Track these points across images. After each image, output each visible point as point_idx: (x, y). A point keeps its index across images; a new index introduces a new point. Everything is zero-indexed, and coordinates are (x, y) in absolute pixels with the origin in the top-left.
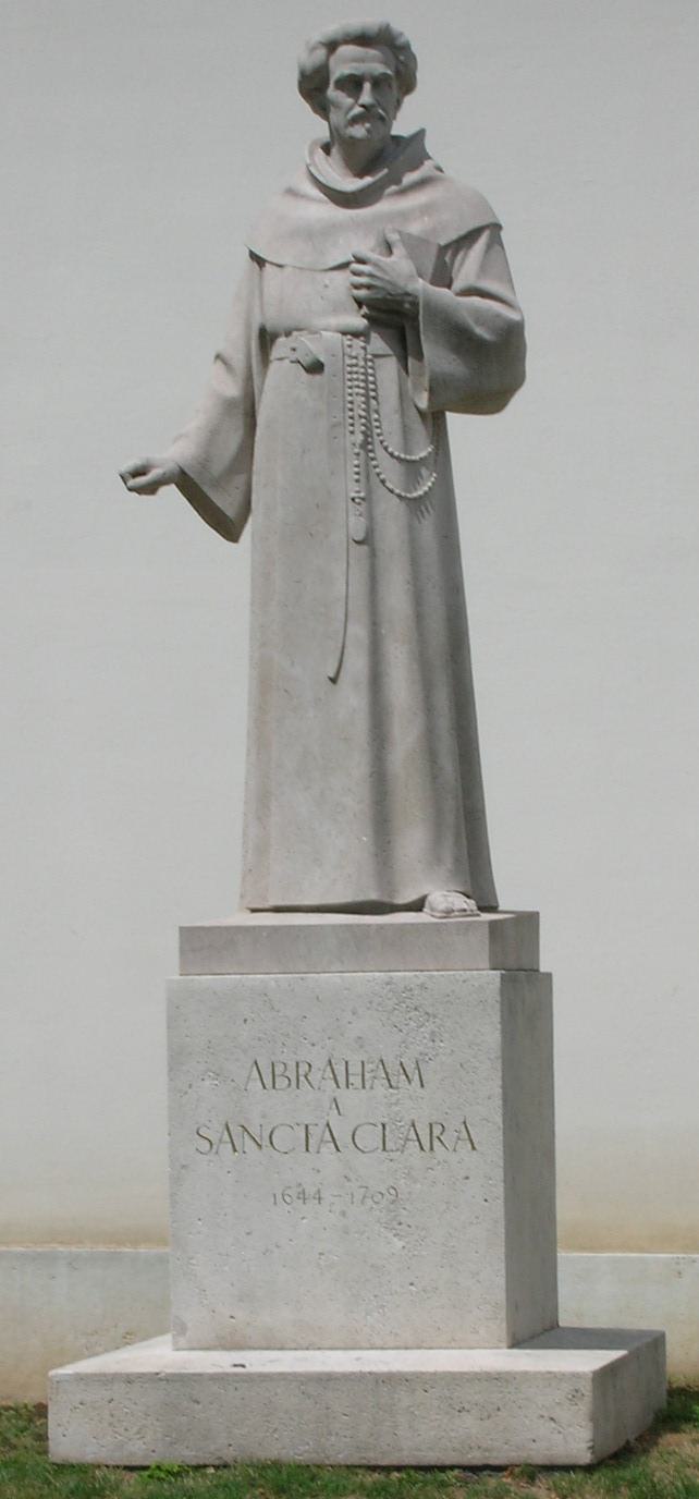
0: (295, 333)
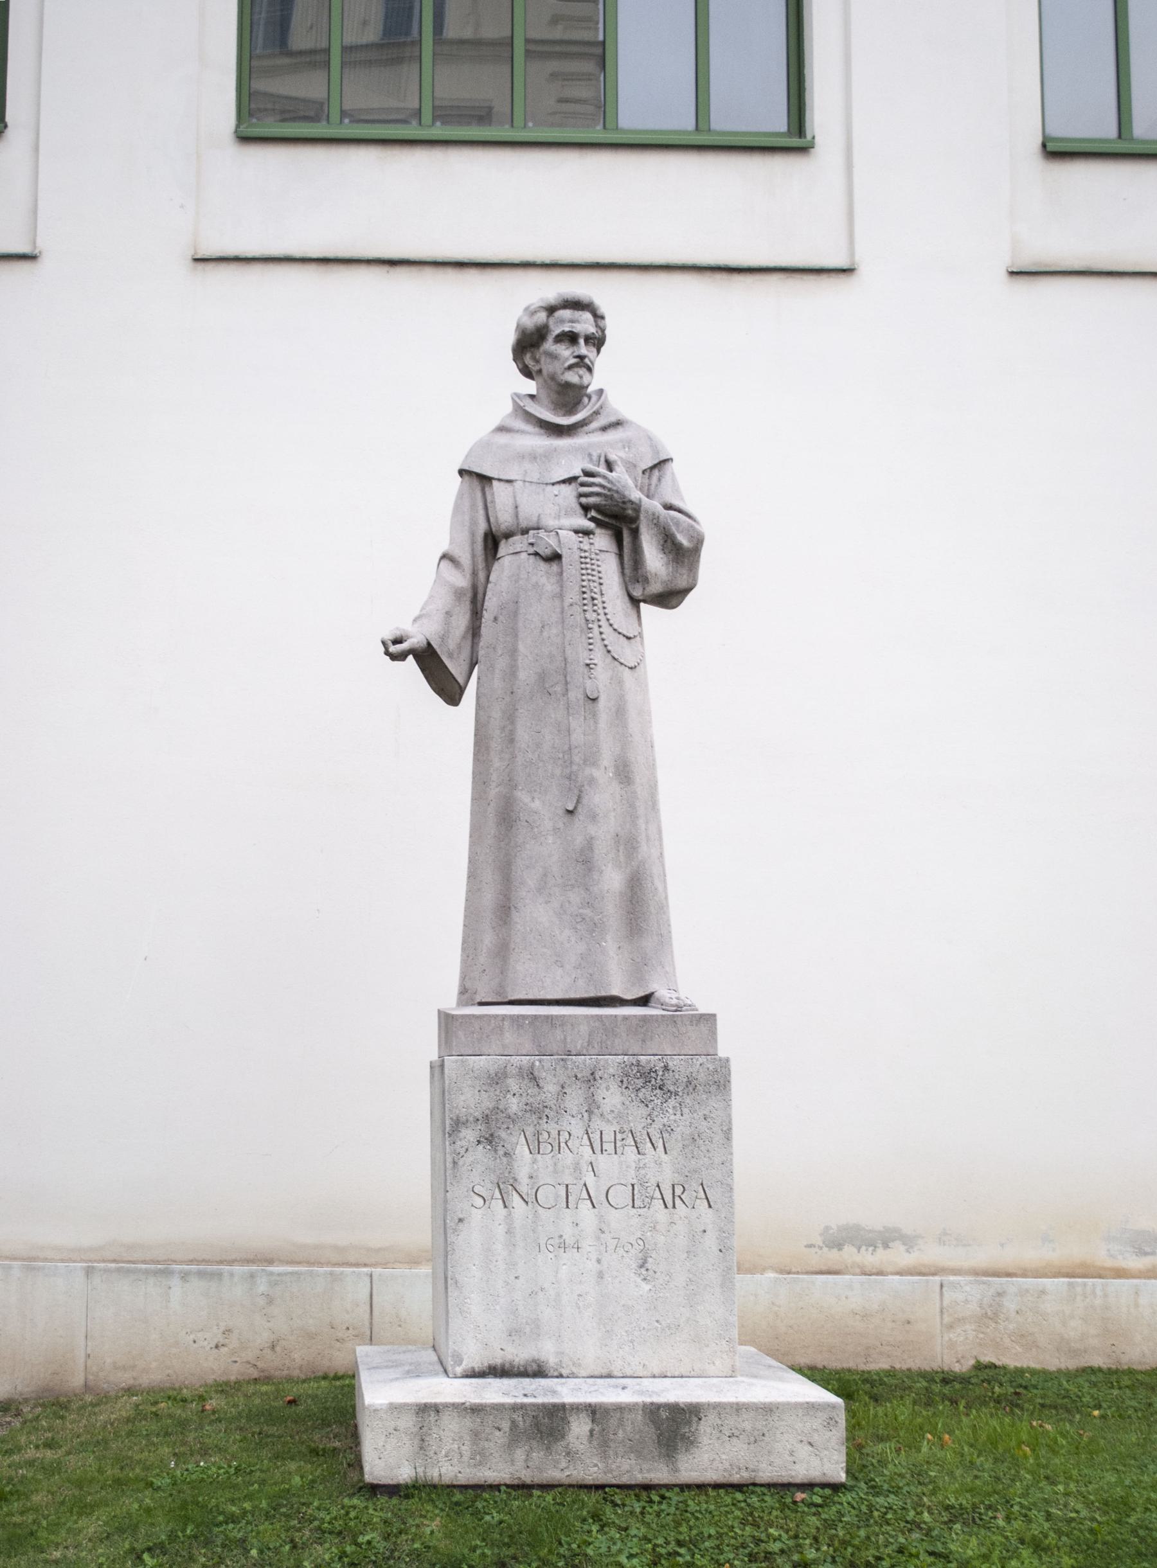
0: (531, 532)
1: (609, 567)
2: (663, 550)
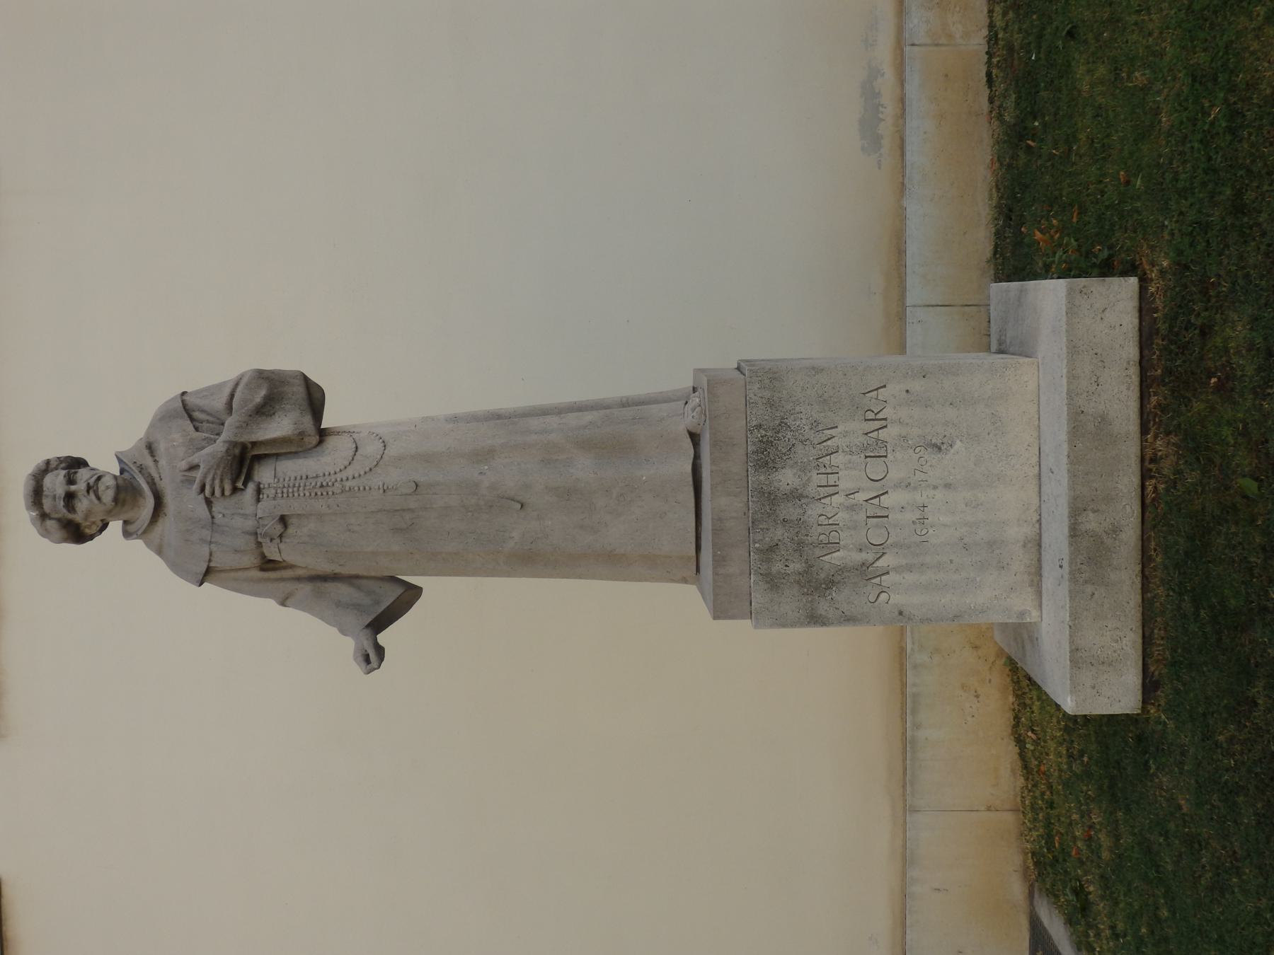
1: (290, 468)
2: (272, 415)
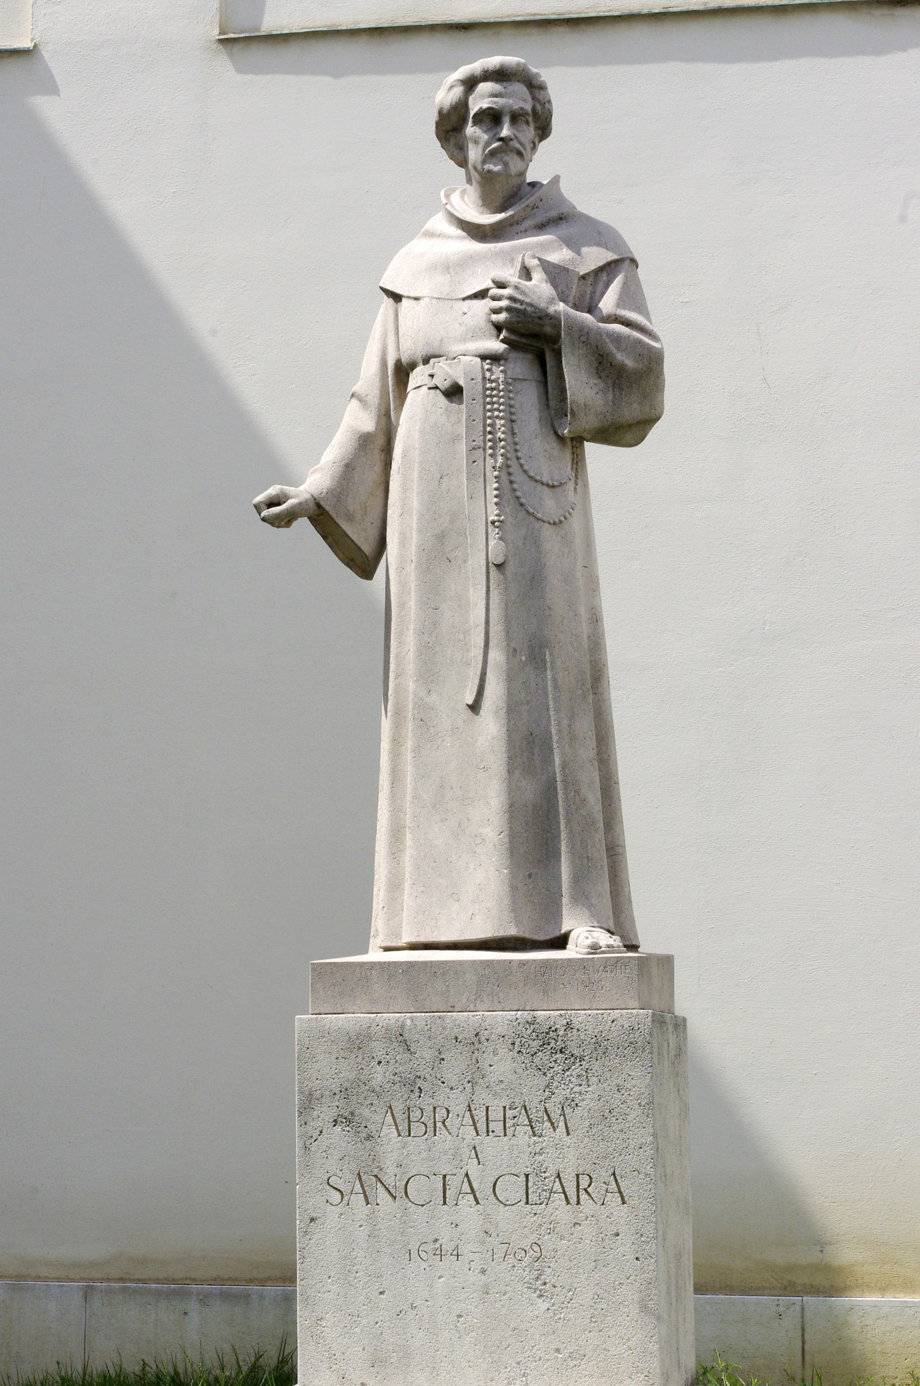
0: (432, 361)
